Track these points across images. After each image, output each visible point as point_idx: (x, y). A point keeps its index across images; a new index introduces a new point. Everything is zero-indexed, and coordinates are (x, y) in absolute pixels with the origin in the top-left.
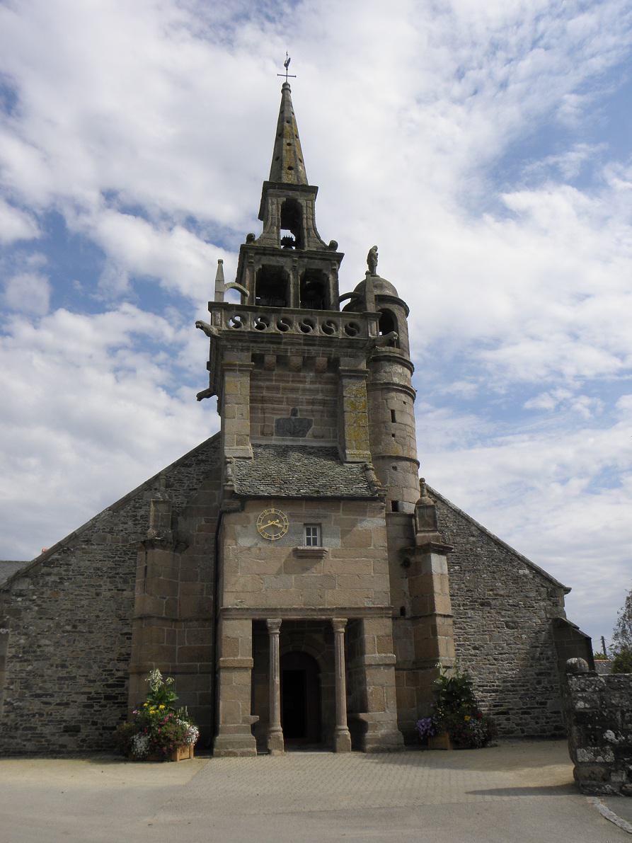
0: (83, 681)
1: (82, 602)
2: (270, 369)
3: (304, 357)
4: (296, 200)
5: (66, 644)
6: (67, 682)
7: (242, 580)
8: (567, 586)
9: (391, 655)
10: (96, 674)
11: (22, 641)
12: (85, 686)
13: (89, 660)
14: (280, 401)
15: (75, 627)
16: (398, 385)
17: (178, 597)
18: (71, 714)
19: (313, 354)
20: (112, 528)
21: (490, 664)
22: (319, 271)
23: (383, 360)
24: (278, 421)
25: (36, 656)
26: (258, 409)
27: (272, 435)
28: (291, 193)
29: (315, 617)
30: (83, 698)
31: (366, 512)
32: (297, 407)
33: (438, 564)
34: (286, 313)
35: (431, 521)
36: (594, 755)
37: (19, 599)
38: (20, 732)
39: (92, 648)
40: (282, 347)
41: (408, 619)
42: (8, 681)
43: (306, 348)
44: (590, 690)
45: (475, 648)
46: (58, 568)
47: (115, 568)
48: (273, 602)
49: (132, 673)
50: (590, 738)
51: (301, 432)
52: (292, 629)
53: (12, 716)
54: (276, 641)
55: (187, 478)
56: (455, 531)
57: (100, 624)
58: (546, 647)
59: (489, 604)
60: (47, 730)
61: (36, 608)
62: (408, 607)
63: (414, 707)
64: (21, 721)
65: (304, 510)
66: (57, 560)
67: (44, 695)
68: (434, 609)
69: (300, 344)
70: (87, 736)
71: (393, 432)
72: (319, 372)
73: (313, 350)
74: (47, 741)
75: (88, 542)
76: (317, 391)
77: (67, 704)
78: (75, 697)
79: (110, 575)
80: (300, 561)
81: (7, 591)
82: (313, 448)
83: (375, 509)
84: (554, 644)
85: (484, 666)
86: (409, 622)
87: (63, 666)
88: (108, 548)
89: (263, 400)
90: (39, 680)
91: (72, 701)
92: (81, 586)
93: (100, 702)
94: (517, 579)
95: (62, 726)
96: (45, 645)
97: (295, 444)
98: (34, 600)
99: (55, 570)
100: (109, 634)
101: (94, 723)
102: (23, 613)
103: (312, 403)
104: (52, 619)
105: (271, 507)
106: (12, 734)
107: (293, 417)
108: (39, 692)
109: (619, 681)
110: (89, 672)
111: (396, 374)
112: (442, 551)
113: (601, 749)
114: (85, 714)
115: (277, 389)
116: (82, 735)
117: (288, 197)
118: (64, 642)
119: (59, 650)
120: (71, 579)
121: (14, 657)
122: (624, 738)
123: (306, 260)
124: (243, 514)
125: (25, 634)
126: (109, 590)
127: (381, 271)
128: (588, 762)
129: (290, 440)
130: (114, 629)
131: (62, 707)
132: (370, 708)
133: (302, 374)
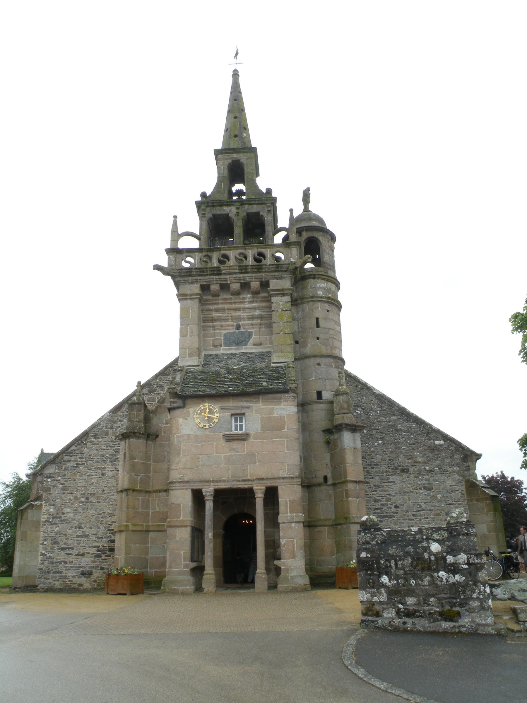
0: (94, 538)
1: (93, 481)
2: (216, 295)
3: (241, 283)
4: (239, 161)
5: (82, 512)
6: (83, 539)
7: (183, 460)
8: (478, 452)
9: (300, 514)
10: (102, 533)
11: (52, 510)
12: (95, 541)
13: (98, 522)
14: (226, 320)
15: (87, 499)
16: (321, 297)
17: (151, 475)
18: (86, 562)
19: (248, 280)
20: (112, 425)
21: (409, 520)
22: (258, 214)
23: (309, 278)
24: (225, 335)
25: (61, 521)
26: (210, 327)
27: (221, 346)
28: (235, 155)
29: (240, 486)
30: (94, 551)
31: (281, 402)
32: (240, 323)
33: (349, 441)
34: (224, 250)
35: (345, 406)
36: (371, 596)
37: (49, 480)
38: (52, 575)
39: (100, 514)
40: (223, 277)
41: (329, 485)
42: (43, 539)
43: (241, 275)
44: (374, 542)
45: (396, 507)
46: (75, 457)
47: (115, 455)
48: (207, 475)
49: (320, 485)
50: (369, 581)
51: (244, 342)
52: (220, 495)
53: (46, 563)
54: (209, 505)
55: (166, 384)
56: (379, 412)
57: (105, 496)
58: (459, 504)
59: (407, 471)
60: (70, 574)
61: (61, 486)
62: (330, 476)
63: (333, 555)
64: (52, 567)
65: (231, 403)
66: (75, 450)
67: (67, 548)
68: (346, 476)
69: (236, 273)
70: (97, 578)
71: (318, 336)
72: (256, 293)
73: (247, 277)
74: (70, 581)
75: (95, 436)
76: (255, 308)
77: (83, 555)
78: (88, 550)
79: (112, 460)
80: (228, 443)
81: (41, 474)
82: (252, 353)
83: (289, 399)
84: (466, 501)
85: (403, 521)
86: (331, 487)
87: (80, 527)
88: (110, 440)
89: (213, 320)
90: (63, 537)
91: (87, 553)
92: (91, 469)
93: (106, 553)
94: (434, 449)
95: (80, 571)
96: (67, 513)
97: (238, 352)
98: (59, 480)
99: (72, 458)
100: (111, 503)
101: (102, 569)
102: (52, 490)
103: (252, 318)
104: (72, 493)
105: (206, 403)
106: (46, 576)
107: (237, 331)
108: (64, 546)
109: (398, 535)
110: (98, 532)
111: (320, 287)
112: (354, 428)
113: (377, 590)
114: (95, 562)
115: (223, 310)
116: (93, 578)
117: (237, 160)
118: (80, 510)
119: (77, 516)
120: (84, 464)
121: (47, 521)
122: (396, 582)
123: (246, 206)
124: (184, 410)
125: (54, 505)
126: (111, 471)
127: (312, 207)
128: (366, 601)
129: (235, 349)
130: (115, 500)
131: (79, 557)
132: (282, 556)
133: (241, 296)
